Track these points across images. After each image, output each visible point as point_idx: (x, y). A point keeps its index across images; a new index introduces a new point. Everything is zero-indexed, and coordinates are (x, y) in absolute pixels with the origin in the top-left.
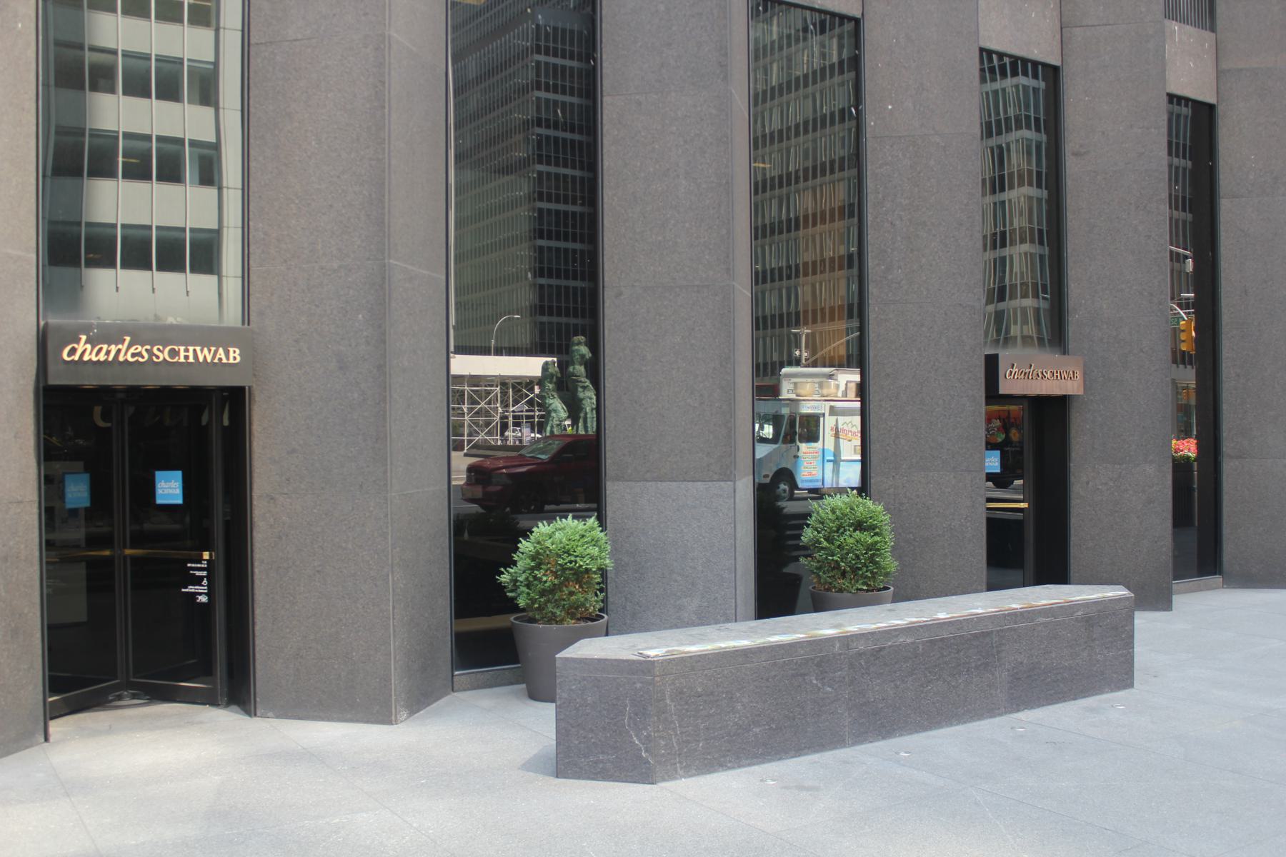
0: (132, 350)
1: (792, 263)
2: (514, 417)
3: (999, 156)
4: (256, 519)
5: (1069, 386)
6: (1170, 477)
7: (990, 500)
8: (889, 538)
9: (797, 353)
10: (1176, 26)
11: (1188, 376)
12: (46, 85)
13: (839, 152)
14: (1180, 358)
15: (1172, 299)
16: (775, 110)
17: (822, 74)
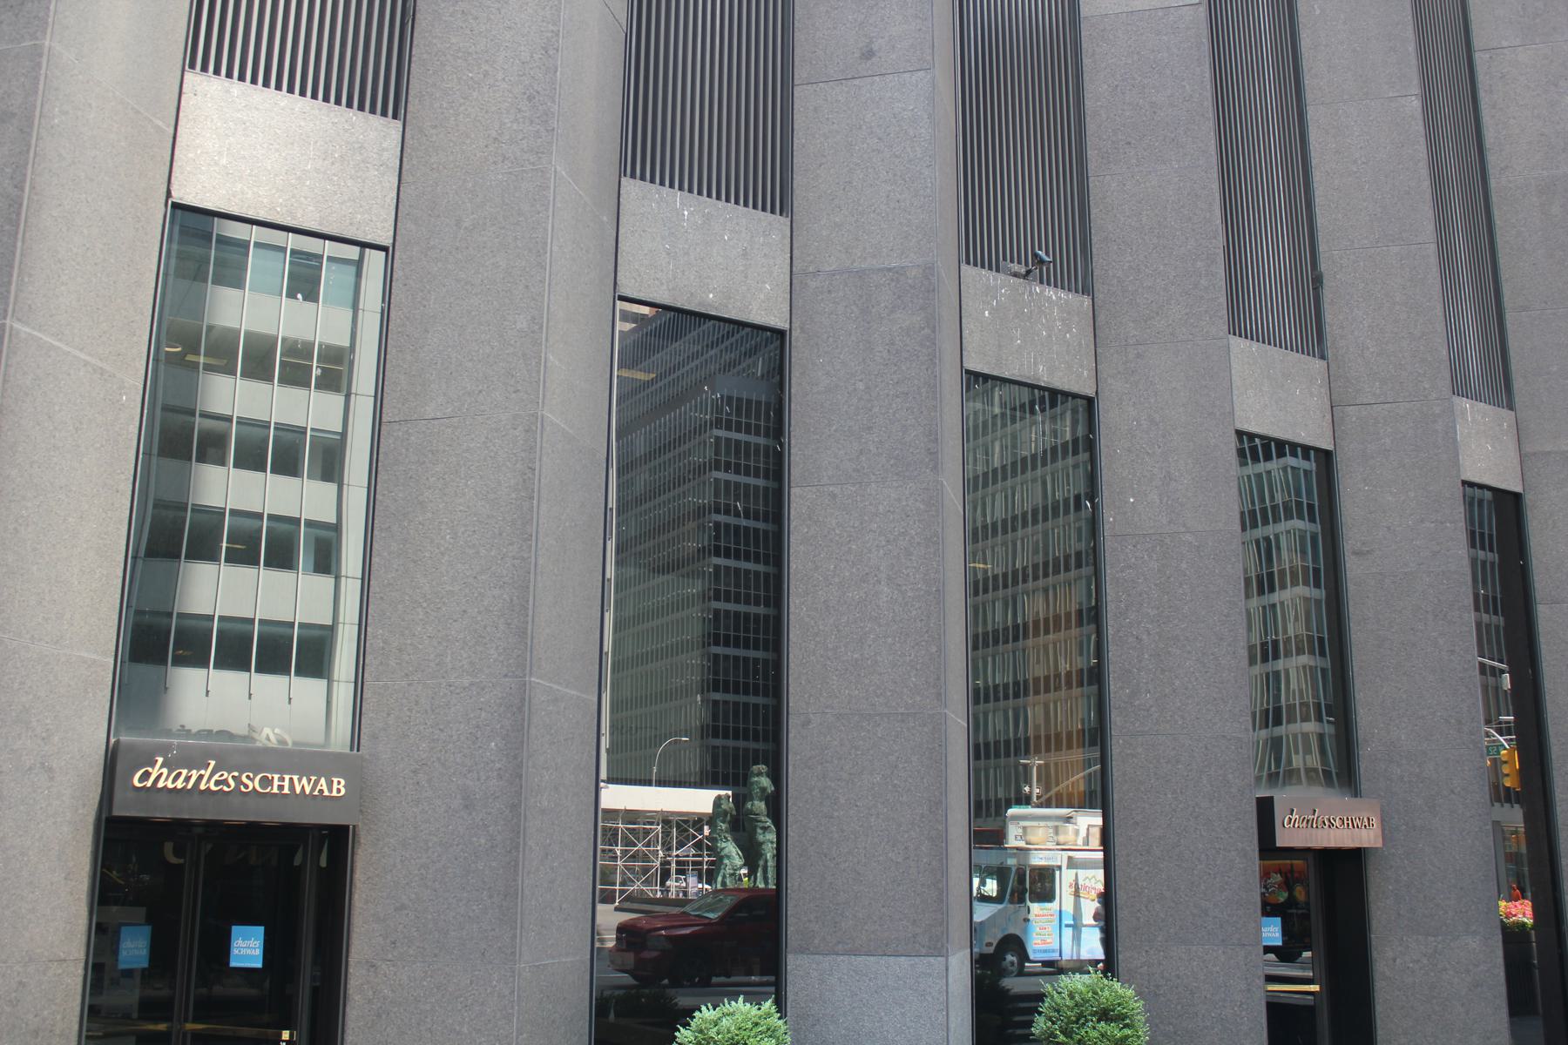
0: (216, 777)
1: (1020, 678)
2: (678, 863)
3: (1267, 550)
4: (350, 991)
5: (1366, 836)
6: (1500, 953)
7: (1271, 979)
8: (1143, 1031)
9: (1027, 789)
10: (1467, 404)
11: (1514, 817)
12: (147, 454)
13: (1074, 546)
14: (1501, 795)
15: (1488, 722)
16: (998, 496)
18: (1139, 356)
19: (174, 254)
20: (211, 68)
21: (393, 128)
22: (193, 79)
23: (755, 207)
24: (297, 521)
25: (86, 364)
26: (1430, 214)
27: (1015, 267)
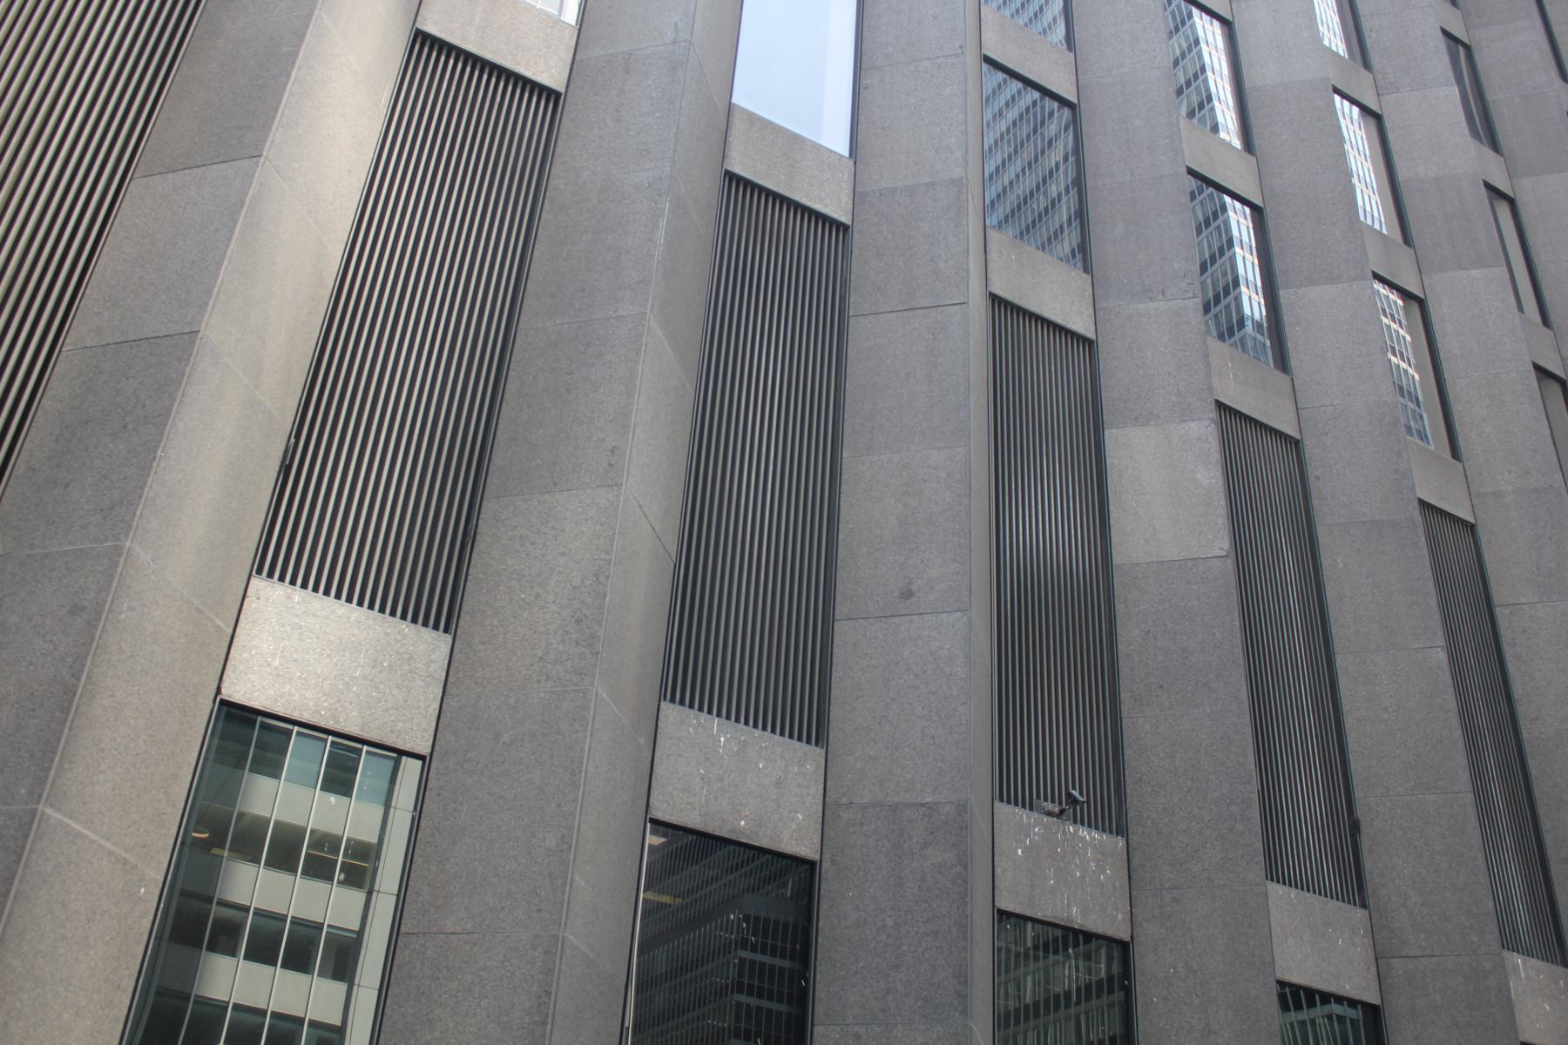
12: (159, 939)
17: (1087, 992)
18: (1174, 900)
19: (214, 748)
20: (277, 575)
22: (258, 583)
23: (791, 736)
24: (301, 1021)
25: (110, 853)
26: (1464, 763)
27: (1049, 806)
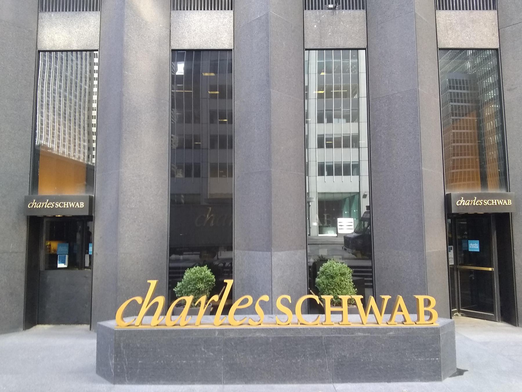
21: (362, 12)
27: (331, 6)
